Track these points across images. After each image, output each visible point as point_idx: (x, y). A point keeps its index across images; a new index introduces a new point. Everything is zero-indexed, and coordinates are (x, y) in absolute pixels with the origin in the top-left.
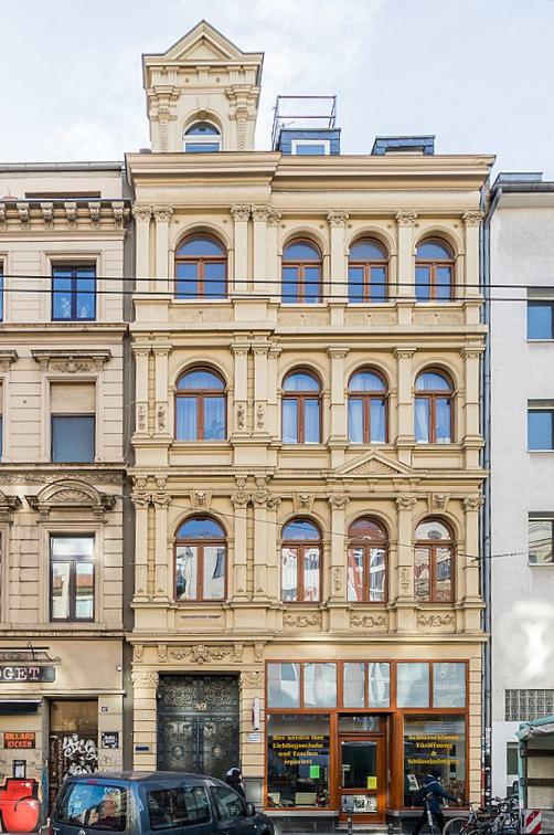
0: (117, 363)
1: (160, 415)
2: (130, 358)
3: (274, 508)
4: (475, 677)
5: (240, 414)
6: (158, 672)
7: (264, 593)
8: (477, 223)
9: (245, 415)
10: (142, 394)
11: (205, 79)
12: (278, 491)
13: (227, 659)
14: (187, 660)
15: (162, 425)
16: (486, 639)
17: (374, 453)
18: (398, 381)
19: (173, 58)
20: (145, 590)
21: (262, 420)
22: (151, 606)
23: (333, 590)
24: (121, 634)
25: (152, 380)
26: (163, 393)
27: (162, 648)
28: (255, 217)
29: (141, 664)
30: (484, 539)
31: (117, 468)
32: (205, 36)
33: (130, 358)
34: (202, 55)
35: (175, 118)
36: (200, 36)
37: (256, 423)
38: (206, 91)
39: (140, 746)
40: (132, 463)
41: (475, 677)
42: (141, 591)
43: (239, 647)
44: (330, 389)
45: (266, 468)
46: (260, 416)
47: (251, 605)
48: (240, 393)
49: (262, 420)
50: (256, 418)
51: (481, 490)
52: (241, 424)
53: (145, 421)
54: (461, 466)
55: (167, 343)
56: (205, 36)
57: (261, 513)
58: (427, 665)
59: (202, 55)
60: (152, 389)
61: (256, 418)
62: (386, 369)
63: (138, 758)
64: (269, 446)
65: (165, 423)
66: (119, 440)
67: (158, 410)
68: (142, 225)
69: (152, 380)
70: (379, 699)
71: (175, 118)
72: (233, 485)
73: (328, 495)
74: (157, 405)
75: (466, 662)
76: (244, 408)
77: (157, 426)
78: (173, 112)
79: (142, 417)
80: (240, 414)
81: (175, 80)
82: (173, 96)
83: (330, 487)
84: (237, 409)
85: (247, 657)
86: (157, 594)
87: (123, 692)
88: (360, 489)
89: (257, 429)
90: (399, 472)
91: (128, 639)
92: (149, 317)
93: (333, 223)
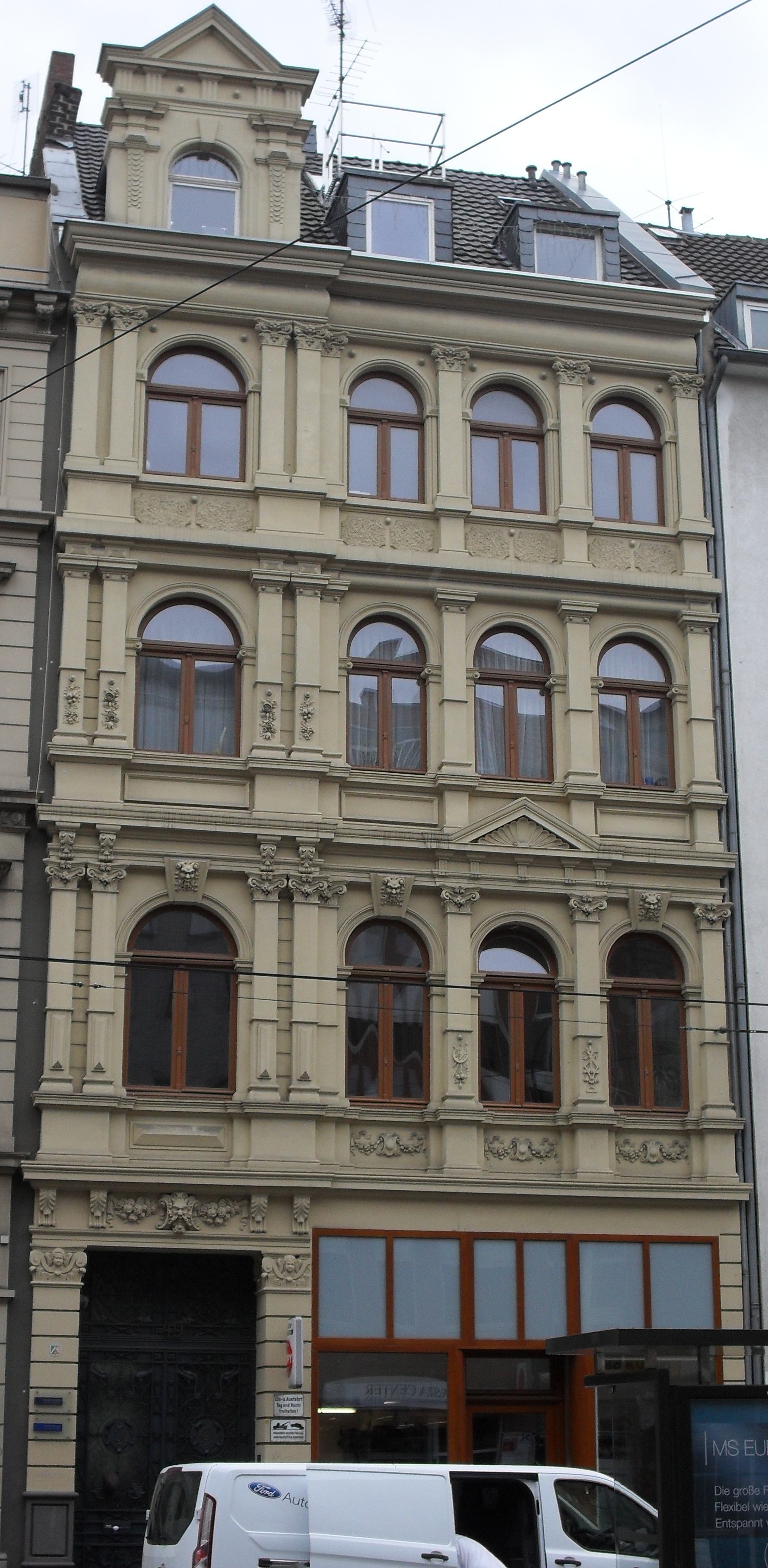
0: (26, 583)
1: (110, 698)
2: (51, 583)
3: (334, 902)
4: (730, 1275)
5: (267, 709)
6: (91, 1252)
7: (312, 1085)
8: (694, 392)
9: (277, 712)
10: (73, 653)
11: (211, 92)
12: (345, 870)
13: (234, 1228)
14: (148, 1226)
15: (111, 718)
16: (745, 1197)
17: (525, 807)
18: (566, 662)
19: (157, 56)
20: (66, 1065)
21: (309, 725)
22: (79, 1106)
23: (451, 1081)
24: (12, 1163)
25: (96, 622)
26: (116, 656)
27: (99, 1196)
28: (301, 341)
29: (49, 1231)
30: (736, 984)
31: (19, 800)
32: (214, 26)
33: (51, 583)
34: (209, 56)
35: (156, 149)
36: (207, 25)
37: (298, 728)
38: (216, 111)
39: (43, 1393)
40: (48, 795)
41: (730, 1275)
42: (57, 1067)
43: (259, 1201)
44: (255, 650)
45: (317, 827)
46: (307, 716)
47: (285, 1114)
48: (267, 666)
49: (309, 725)
50: (299, 719)
51: (725, 890)
52: (269, 729)
53: (79, 709)
54: (688, 838)
55: (132, 559)
56: (214, 26)
57: (307, 916)
58: (636, 1250)
59: (209, 56)
60: (95, 641)
61: (299, 719)
62: (669, 651)
63: (36, 1452)
64: (323, 779)
65: (118, 713)
66: (21, 739)
67: (104, 687)
68: (88, 335)
69: (96, 622)
70: (546, 1325)
71: (156, 149)
72: (251, 855)
73: (439, 883)
74: (104, 679)
75: (712, 1242)
76: (277, 697)
77: (101, 719)
78: (152, 138)
79: (72, 700)
80: (267, 709)
81: (155, 88)
82: (154, 113)
83: (443, 868)
84: (261, 698)
85: (277, 1226)
86: (89, 1076)
87: (11, 1294)
88: (500, 877)
89: (299, 743)
90: (572, 847)
91: (27, 1176)
92: (80, 792)
93: (443, 364)
